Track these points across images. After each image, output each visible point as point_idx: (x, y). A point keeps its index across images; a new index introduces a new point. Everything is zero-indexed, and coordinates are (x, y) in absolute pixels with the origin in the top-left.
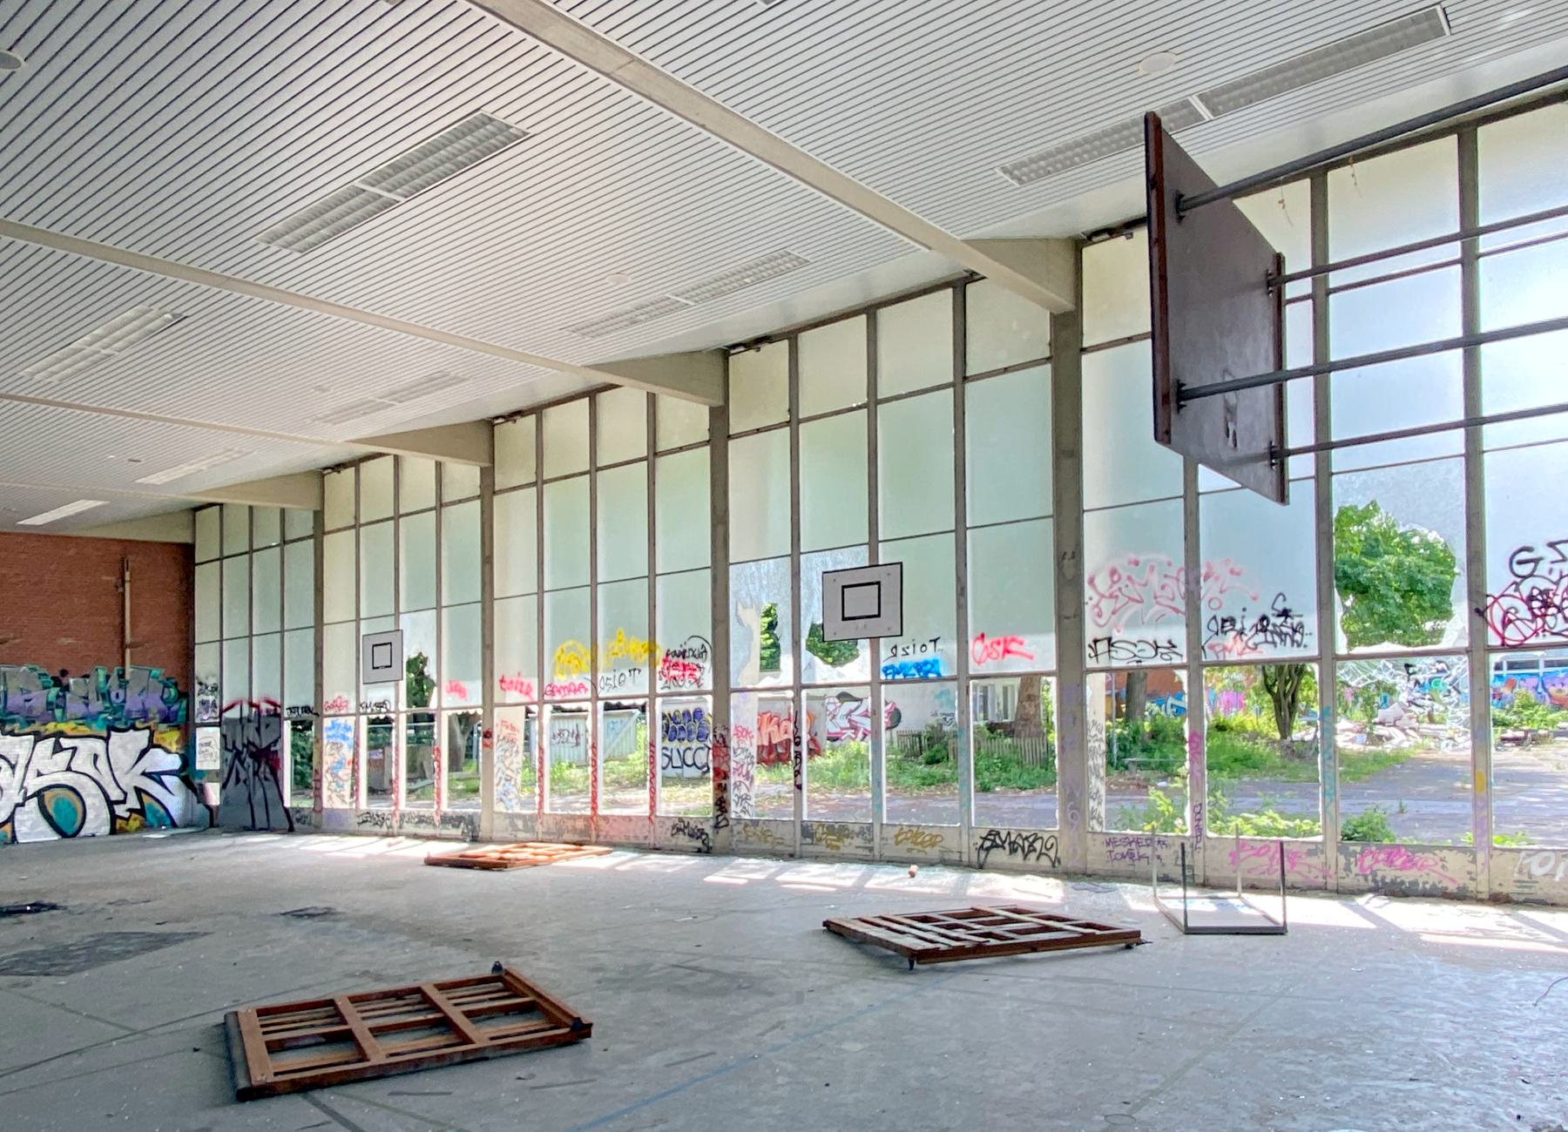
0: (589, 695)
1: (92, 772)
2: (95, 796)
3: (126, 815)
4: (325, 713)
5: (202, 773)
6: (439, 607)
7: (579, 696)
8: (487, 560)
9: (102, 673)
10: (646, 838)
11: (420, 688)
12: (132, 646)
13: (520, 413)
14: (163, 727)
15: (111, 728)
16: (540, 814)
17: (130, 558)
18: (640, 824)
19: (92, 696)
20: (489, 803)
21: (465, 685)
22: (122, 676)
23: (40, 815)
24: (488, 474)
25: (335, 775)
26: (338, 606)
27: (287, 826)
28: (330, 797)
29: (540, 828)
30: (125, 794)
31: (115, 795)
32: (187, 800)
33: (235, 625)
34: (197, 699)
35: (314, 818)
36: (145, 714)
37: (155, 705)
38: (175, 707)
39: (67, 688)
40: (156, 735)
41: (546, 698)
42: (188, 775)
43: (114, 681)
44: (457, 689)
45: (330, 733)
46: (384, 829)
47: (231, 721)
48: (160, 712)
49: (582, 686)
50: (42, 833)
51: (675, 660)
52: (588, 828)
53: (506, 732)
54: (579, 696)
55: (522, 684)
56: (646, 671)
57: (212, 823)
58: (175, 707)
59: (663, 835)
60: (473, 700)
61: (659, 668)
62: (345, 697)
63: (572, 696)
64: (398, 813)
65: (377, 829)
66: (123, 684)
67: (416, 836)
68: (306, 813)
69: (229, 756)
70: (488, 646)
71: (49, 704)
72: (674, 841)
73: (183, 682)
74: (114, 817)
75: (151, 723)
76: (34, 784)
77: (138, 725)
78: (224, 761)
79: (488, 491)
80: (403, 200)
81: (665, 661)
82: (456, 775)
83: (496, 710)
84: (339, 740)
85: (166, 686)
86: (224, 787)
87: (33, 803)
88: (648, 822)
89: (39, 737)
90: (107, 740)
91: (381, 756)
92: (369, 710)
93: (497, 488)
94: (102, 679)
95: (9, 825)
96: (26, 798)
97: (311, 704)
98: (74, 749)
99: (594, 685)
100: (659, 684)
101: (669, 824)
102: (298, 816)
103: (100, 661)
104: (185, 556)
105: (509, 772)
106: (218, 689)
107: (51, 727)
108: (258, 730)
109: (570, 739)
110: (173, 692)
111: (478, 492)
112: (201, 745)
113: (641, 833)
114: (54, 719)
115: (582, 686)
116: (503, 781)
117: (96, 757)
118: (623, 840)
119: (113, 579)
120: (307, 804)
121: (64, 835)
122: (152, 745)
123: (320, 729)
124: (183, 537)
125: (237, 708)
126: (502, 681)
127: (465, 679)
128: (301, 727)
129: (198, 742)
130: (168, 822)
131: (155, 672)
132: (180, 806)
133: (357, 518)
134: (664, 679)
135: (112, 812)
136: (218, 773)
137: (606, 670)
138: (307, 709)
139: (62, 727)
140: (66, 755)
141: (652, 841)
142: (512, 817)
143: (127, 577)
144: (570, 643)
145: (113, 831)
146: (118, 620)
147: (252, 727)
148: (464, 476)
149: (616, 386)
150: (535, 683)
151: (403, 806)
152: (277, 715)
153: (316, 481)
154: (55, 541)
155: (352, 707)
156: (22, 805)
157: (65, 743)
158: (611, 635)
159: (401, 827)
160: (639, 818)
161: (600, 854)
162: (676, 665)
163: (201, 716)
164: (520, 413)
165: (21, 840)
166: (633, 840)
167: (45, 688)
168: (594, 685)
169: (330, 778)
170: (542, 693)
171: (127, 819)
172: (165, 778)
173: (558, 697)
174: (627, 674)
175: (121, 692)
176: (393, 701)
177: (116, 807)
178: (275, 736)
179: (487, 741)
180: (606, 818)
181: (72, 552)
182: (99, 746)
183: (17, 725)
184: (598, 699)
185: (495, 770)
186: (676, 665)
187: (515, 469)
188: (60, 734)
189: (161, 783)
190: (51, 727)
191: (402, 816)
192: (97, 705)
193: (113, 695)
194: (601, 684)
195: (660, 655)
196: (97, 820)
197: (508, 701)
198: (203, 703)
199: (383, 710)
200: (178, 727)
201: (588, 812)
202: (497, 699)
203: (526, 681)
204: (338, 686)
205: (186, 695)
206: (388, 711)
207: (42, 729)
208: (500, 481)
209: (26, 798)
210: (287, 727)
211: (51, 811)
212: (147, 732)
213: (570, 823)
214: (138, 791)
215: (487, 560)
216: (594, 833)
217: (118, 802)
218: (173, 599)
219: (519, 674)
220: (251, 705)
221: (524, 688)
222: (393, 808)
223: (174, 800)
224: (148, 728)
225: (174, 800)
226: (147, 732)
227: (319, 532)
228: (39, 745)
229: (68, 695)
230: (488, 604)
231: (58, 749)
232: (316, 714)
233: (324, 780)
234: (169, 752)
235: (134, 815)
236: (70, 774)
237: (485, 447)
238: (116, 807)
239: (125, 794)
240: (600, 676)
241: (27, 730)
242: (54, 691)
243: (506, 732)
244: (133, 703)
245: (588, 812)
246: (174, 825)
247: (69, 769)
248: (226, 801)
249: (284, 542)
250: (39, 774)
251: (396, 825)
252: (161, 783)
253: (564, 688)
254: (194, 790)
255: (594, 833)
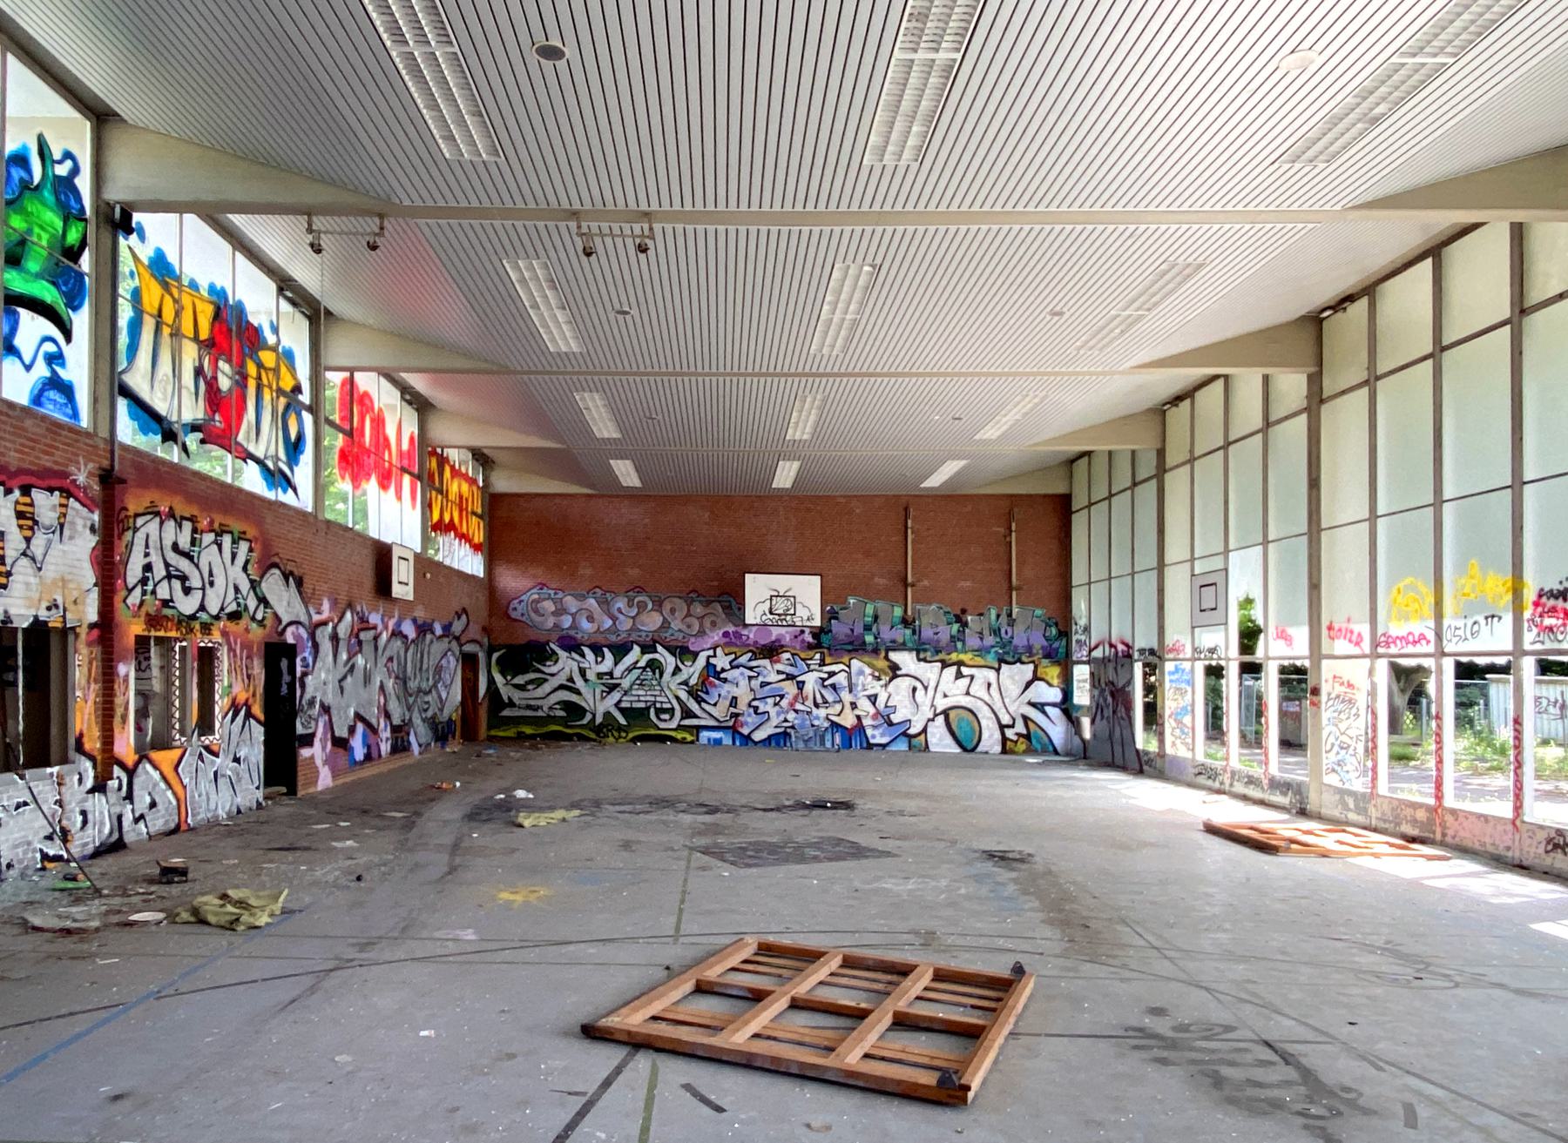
0: (1431, 649)
1: (987, 698)
2: (988, 718)
3: (1015, 738)
4: (1167, 656)
5: (1080, 707)
6: (1265, 542)
7: (1419, 649)
8: (1314, 483)
9: (993, 613)
10: (1508, 848)
11: (1250, 636)
12: (1018, 589)
13: (1350, 298)
14: (1045, 662)
15: (1002, 661)
16: (1373, 795)
17: (1016, 510)
18: (1500, 828)
19: (986, 632)
20: (1317, 773)
21: (1291, 631)
22: (1010, 615)
23: (945, 729)
24: (1315, 381)
25: (1179, 722)
26: (1176, 550)
27: (1138, 768)
28: (1174, 744)
29: (1373, 812)
30: (1014, 720)
31: (1006, 720)
32: (1067, 731)
33: (1099, 572)
34: (1074, 638)
35: (1159, 763)
36: (1029, 650)
37: (1039, 642)
38: (1056, 645)
39: (965, 625)
40: (1040, 670)
41: (1380, 650)
42: (1066, 706)
43: (1004, 619)
44: (1283, 635)
45: (1174, 677)
46: (1217, 785)
47: (1096, 659)
48: (1043, 648)
49: (1423, 637)
50: (946, 746)
51: (1552, 602)
52: (1431, 822)
53: (1339, 689)
54: (1419, 649)
55: (1352, 632)
56: (1508, 618)
57: (1084, 756)
58: (1056, 645)
59: (1533, 851)
60: (1297, 649)
61: (1527, 614)
62: (1183, 641)
63: (1410, 649)
64: (1229, 769)
65: (1209, 783)
66: (1012, 622)
67: (1245, 798)
68: (1152, 756)
69: (1096, 693)
70: (1315, 586)
71: (952, 637)
72: (1548, 860)
73: (1062, 623)
74: (1004, 739)
75: (1035, 658)
76: (942, 704)
77: (1024, 658)
78: (1092, 697)
79: (1317, 399)
80: (1452, 60)
81: (1536, 604)
82: (1395, 738)
83: (1325, 663)
84: (1183, 686)
85: (1048, 625)
86: (1093, 722)
87: (941, 719)
88: (1510, 827)
89: (945, 665)
90: (998, 670)
91: (1298, 709)
92: (1202, 656)
93: (1324, 396)
94: (993, 617)
95: (923, 737)
96: (936, 715)
97: (1155, 646)
98: (972, 677)
99: (1439, 636)
100: (1529, 637)
101: (1542, 836)
102: (1146, 758)
103: (992, 602)
104: (1062, 507)
105: (1344, 738)
106: (1087, 629)
107: (954, 657)
108: (1116, 669)
109: (1551, 709)
110: (1054, 631)
111: (1305, 404)
112: (1079, 681)
113: (1501, 841)
114: (956, 650)
115: (1423, 637)
116: (1336, 748)
117: (989, 685)
118: (1477, 846)
119: (1002, 530)
120: (1153, 747)
121: (964, 749)
122: (1036, 678)
123: (1162, 673)
124: (1060, 488)
125: (1101, 648)
126: (1330, 628)
127: (1292, 625)
128: (1150, 669)
129: (1075, 678)
130: (1051, 748)
131: (1038, 612)
132: (1062, 736)
133: (1192, 451)
134: (1535, 630)
135: (1003, 734)
136: (1089, 708)
137: (1456, 616)
138: (1152, 652)
139: (963, 657)
140: (965, 681)
141: (1517, 854)
142: (1342, 792)
143: (1013, 528)
144: (1408, 580)
145: (1004, 751)
146: (1006, 567)
147: (1111, 667)
148: (1292, 385)
149: (1475, 226)
150: (1364, 629)
151: (1235, 763)
152: (1129, 656)
153: (1158, 419)
154: (949, 499)
155: (1188, 653)
156: (933, 720)
157: (965, 670)
158: (1461, 568)
159: (1231, 785)
160: (1499, 819)
161: (1430, 858)
162: (1553, 610)
163: (1080, 654)
164: (1350, 298)
165: (932, 748)
166: (1490, 849)
167: (949, 624)
168: (1439, 636)
169: (1174, 724)
170: (1375, 644)
171: (1016, 742)
172: (1048, 709)
173: (1393, 650)
174: (1483, 622)
175: (1009, 630)
176: (1223, 648)
177: (1006, 730)
178: (1128, 676)
179: (1314, 698)
180: (1453, 812)
181: (969, 508)
182: (991, 675)
183: (929, 654)
184: (1444, 654)
185: (1325, 734)
186: (1553, 610)
187: (1345, 370)
188: (960, 664)
189: (1044, 713)
190: (954, 657)
191: (1233, 773)
192: (990, 640)
193: (1003, 631)
194: (1447, 635)
195: (1530, 595)
196: (991, 740)
197: (1337, 652)
198: (1078, 641)
199: (1215, 656)
200: (1058, 663)
201: (1432, 801)
202: (1325, 651)
203: (1357, 628)
204: (1176, 633)
205: (1065, 634)
206: (1220, 658)
207: (947, 657)
208: (1329, 387)
209: (936, 715)
210: (1138, 669)
211: (954, 727)
212: (1031, 667)
213: (1409, 812)
214: (1026, 719)
215: (1314, 483)
216: (1438, 830)
217: (1008, 726)
218: (1054, 547)
219: (1349, 620)
220: (1111, 645)
221: (1354, 638)
222: (1224, 763)
223: (1057, 730)
224: (1033, 662)
225: (1057, 730)
226: (1031, 667)
227: (1161, 470)
228: (946, 670)
229: (967, 631)
230: (1315, 534)
231: (959, 675)
232: (1159, 657)
233: (1167, 725)
234: (1050, 685)
235: (1021, 739)
236: (968, 698)
237: (1310, 350)
238: (1006, 730)
239: (1014, 720)
240: (1446, 622)
241: (937, 658)
242: (956, 627)
243: (1339, 689)
244: (1020, 640)
245: (1432, 801)
246: (1056, 752)
247: (968, 693)
248: (1094, 735)
249: (1135, 484)
250: (945, 696)
251: (1227, 782)
252: (1044, 713)
253: (1401, 638)
254: (1072, 722)
255: (1438, 830)
